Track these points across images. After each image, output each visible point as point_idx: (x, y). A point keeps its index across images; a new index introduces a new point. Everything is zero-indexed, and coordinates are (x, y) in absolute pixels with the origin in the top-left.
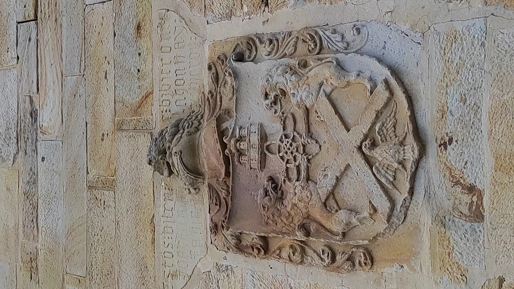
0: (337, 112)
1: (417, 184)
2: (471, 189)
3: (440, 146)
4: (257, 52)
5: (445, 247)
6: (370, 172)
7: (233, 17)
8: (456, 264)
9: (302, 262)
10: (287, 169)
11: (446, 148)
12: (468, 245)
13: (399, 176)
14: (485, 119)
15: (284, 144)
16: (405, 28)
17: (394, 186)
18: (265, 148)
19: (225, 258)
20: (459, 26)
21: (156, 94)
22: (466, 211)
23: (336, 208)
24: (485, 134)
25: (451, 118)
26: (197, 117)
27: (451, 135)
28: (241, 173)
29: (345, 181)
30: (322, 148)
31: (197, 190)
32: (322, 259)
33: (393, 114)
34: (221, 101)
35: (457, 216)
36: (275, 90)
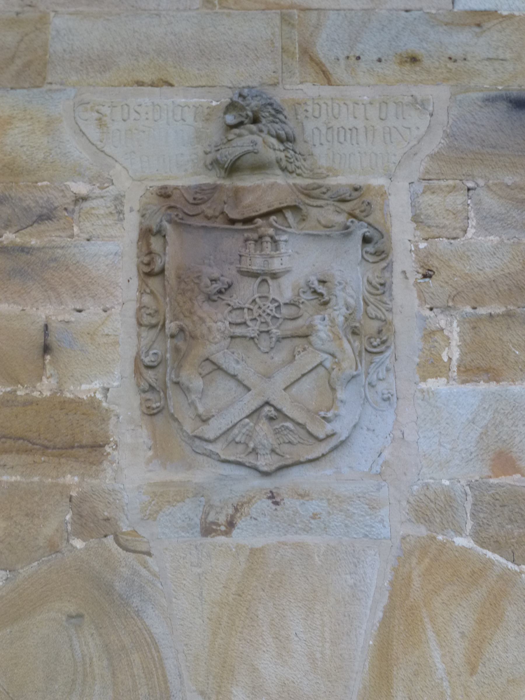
0: (303, 375)
1: (233, 467)
2: (231, 524)
6: (244, 415)
9: (140, 325)
10: (242, 309)
11: (269, 498)
13: (241, 447)
14: (297, 538)
16: (386, 454)
18: (265, 277)
19: (131, 210)
20: (384, 512)
21: (327, 91)
23: (204, 373)
24: (283, 539)
26: (298, 168)
29: (232, 384)
30: (266, 355)
31: (210, 167)
33: (302, 441)
34: (317, 206)
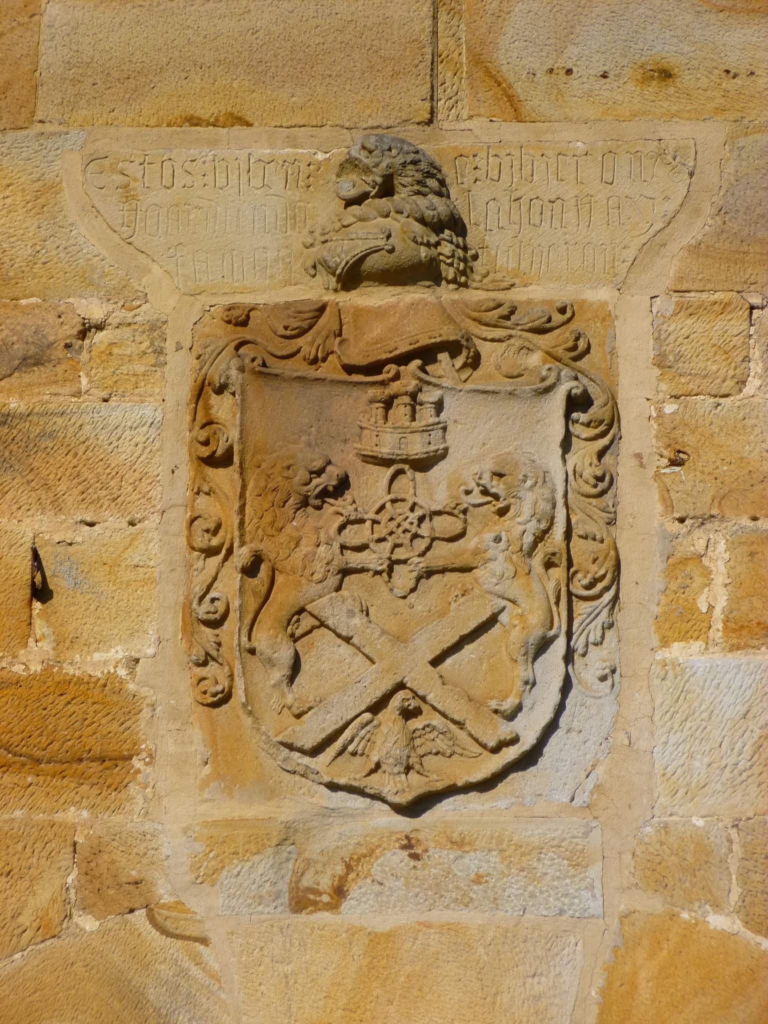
2: (340, 892)
3: (407, 837)
4: (587, 440)
5: (246, 847)
7: (657, 372)
8: (220, 865)
11: (404, 847)
12: (253, 887)
15: (409, 514)
17: (340, 753)
19: (179, 348)
22: (306, 882)
24: (425, 917)
25: (452, 856)
27: (425, 856)
28: (351, 401)
31: (312, 272)
32: (201, 599)
35: (297, 866)
36: (508, 494)
